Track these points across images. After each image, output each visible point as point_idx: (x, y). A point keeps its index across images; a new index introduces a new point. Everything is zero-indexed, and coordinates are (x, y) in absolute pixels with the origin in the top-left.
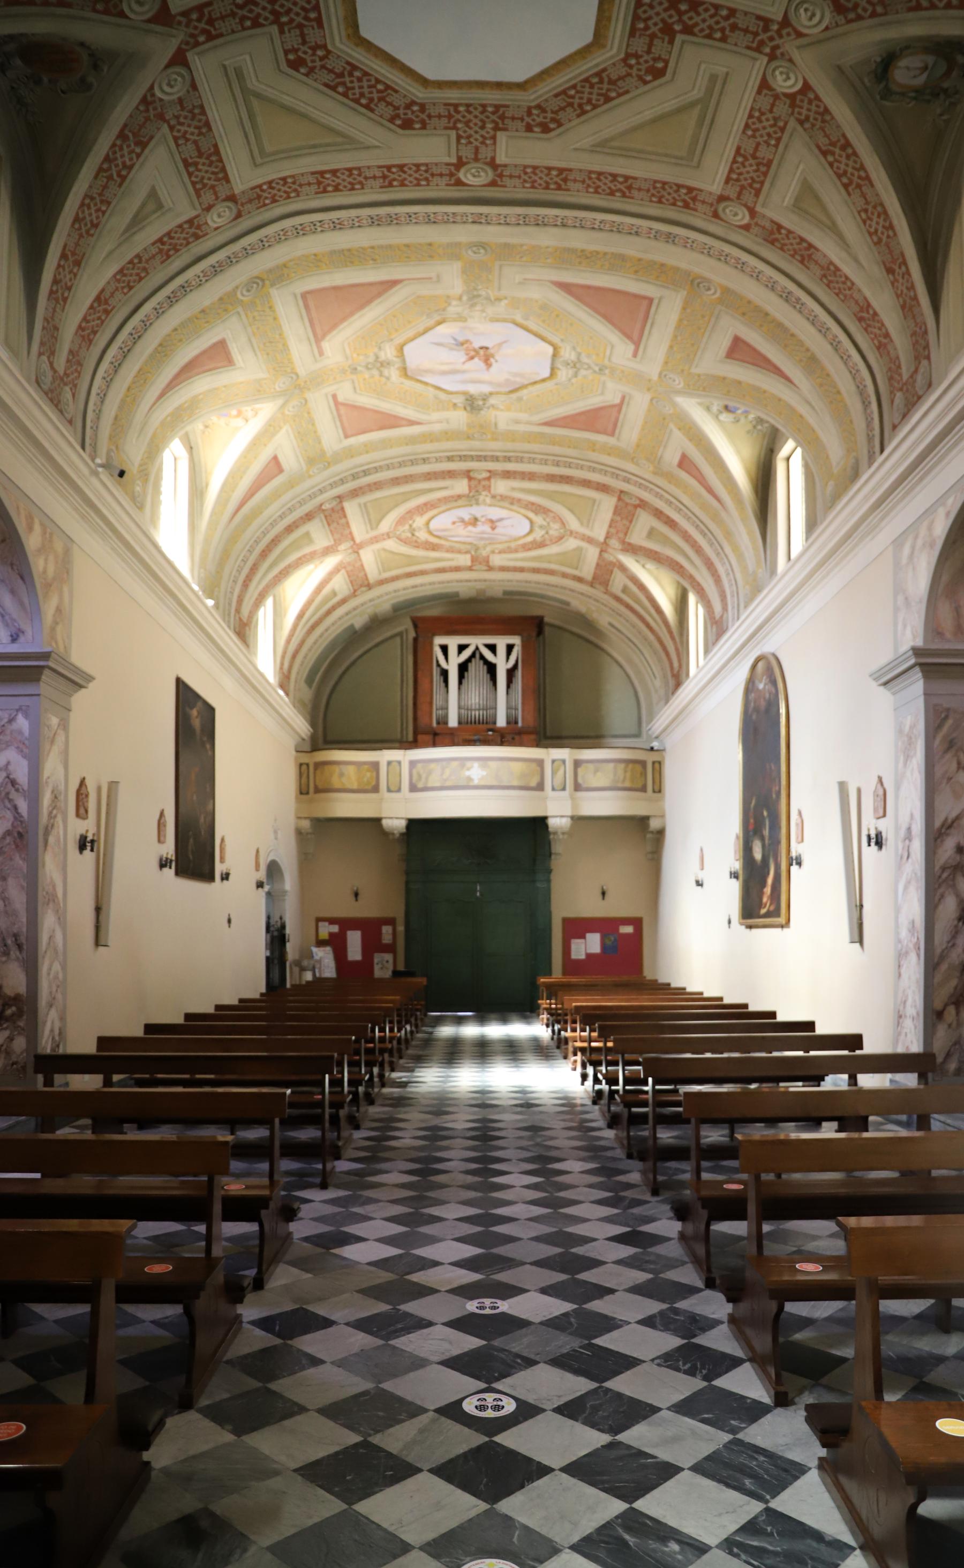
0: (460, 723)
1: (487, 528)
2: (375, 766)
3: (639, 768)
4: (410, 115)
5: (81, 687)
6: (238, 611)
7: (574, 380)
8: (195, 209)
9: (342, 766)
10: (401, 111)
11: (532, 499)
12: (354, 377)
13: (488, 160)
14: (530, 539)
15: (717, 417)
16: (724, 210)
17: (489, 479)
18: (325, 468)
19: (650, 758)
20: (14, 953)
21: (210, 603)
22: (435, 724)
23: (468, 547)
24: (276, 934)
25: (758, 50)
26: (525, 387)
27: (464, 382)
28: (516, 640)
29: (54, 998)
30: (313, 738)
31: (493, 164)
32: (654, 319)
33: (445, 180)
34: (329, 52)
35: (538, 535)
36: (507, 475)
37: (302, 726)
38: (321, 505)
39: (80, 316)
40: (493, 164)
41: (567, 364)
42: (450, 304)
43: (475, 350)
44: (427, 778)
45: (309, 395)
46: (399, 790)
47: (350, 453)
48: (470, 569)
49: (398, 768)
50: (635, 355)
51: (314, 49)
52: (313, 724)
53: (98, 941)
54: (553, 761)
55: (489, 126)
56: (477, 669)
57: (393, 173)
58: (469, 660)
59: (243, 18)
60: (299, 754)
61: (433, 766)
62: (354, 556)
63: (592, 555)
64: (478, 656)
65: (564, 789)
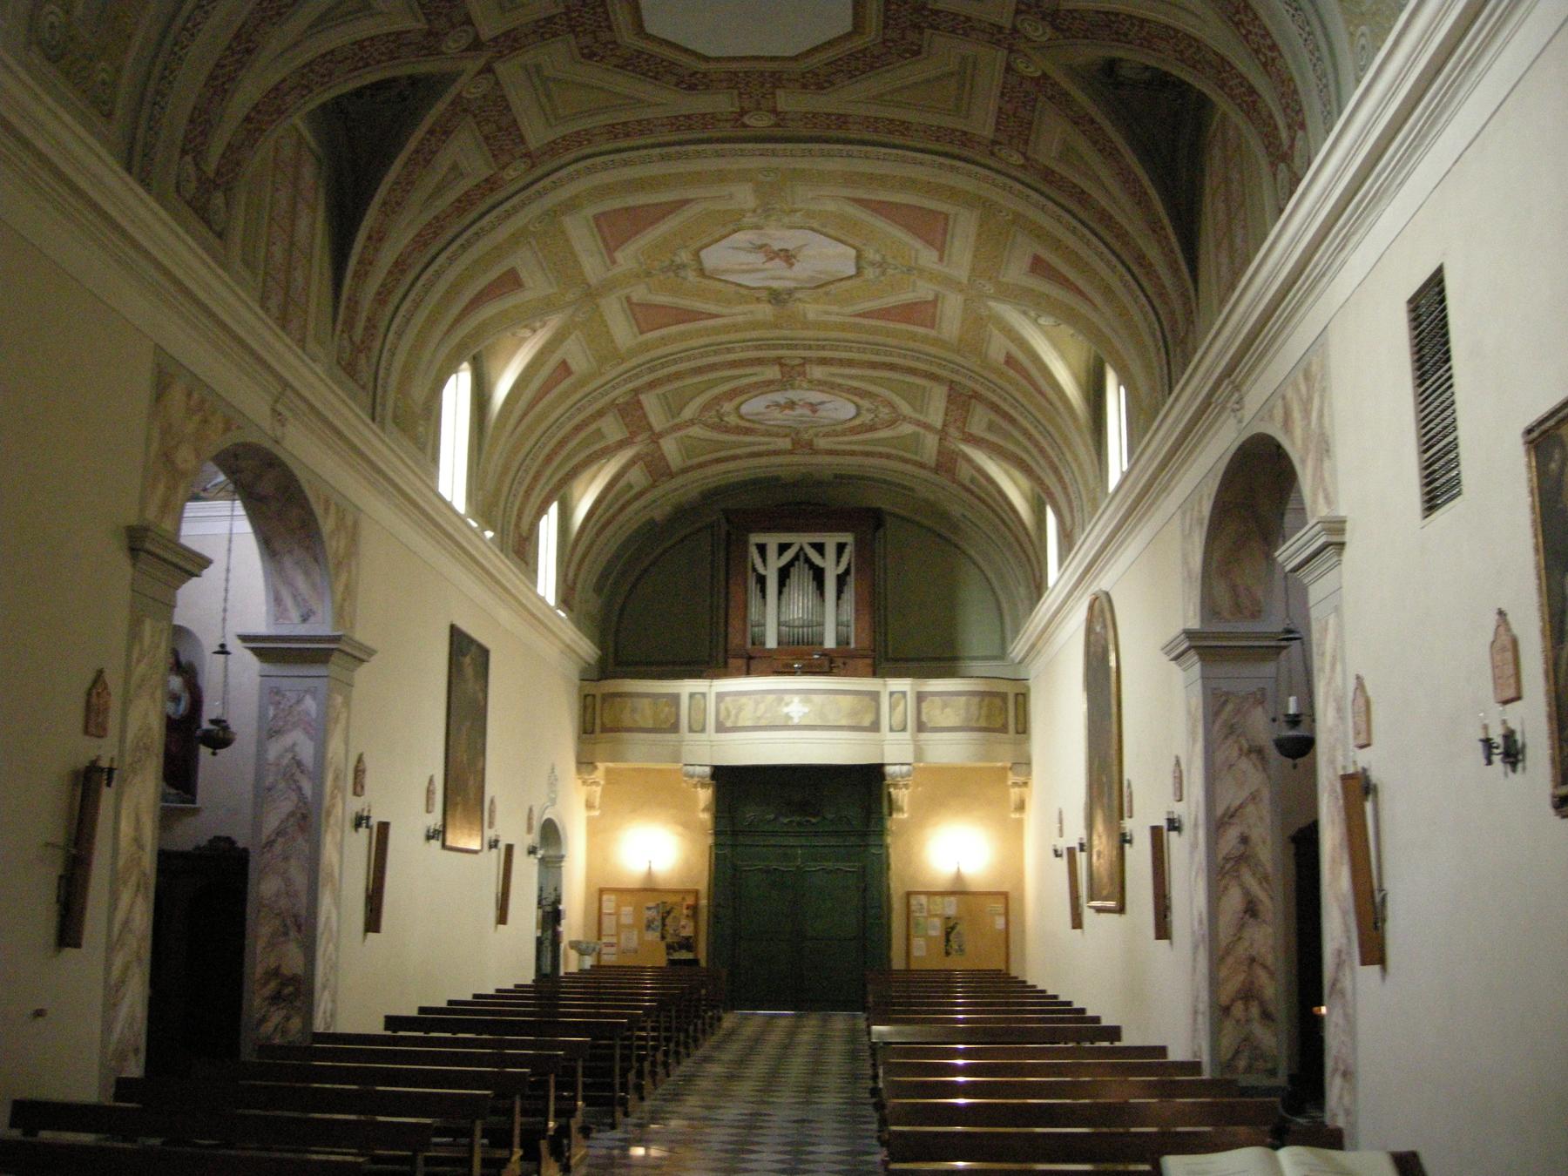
0: (779, 643)
1: (807, 412)
2: (675, 699)
3: (998, 701)
5: (362, 661)
6: (517, 526)
7: (882, 278)
9: (635, 700)
11: (855, 384)
12: (647, 280)
14: (857, 422)
15: (1036, 320)
16: (1000, 150)
17: (803, 365)
18: (619, 364)
19: (1009, 689)
20: (293, 934)
21: (489, 534)
22: (749, 646)
23: (788, 431)
24: (549, 909)
27: (767, 279)
28: (848, 538)
29: (328, 980)
30: (602, 661)
31: (774, 111)
35: (867, 418)
36: (823, 362)
37: (587, 649)
38: (615, 400)
39: (379, 282)
40: (774, 111)
41: (872, 264)
42: (744, 216)
43: (774, 252)
44: (737, 716)
45: (603, 302)
46: (703, 730)
47: (645, 347)
48: (791, 452)
49: (702, 702)
52: (601, 645)
53: (373, 922)
54: (892, 694)
56: (802, 577)
58: (791, 564)
60: (586, 683)
61: (744, 700)
62: (652, 446)
63: (931, 442)
64: (802, 558)
65: (904, 729)
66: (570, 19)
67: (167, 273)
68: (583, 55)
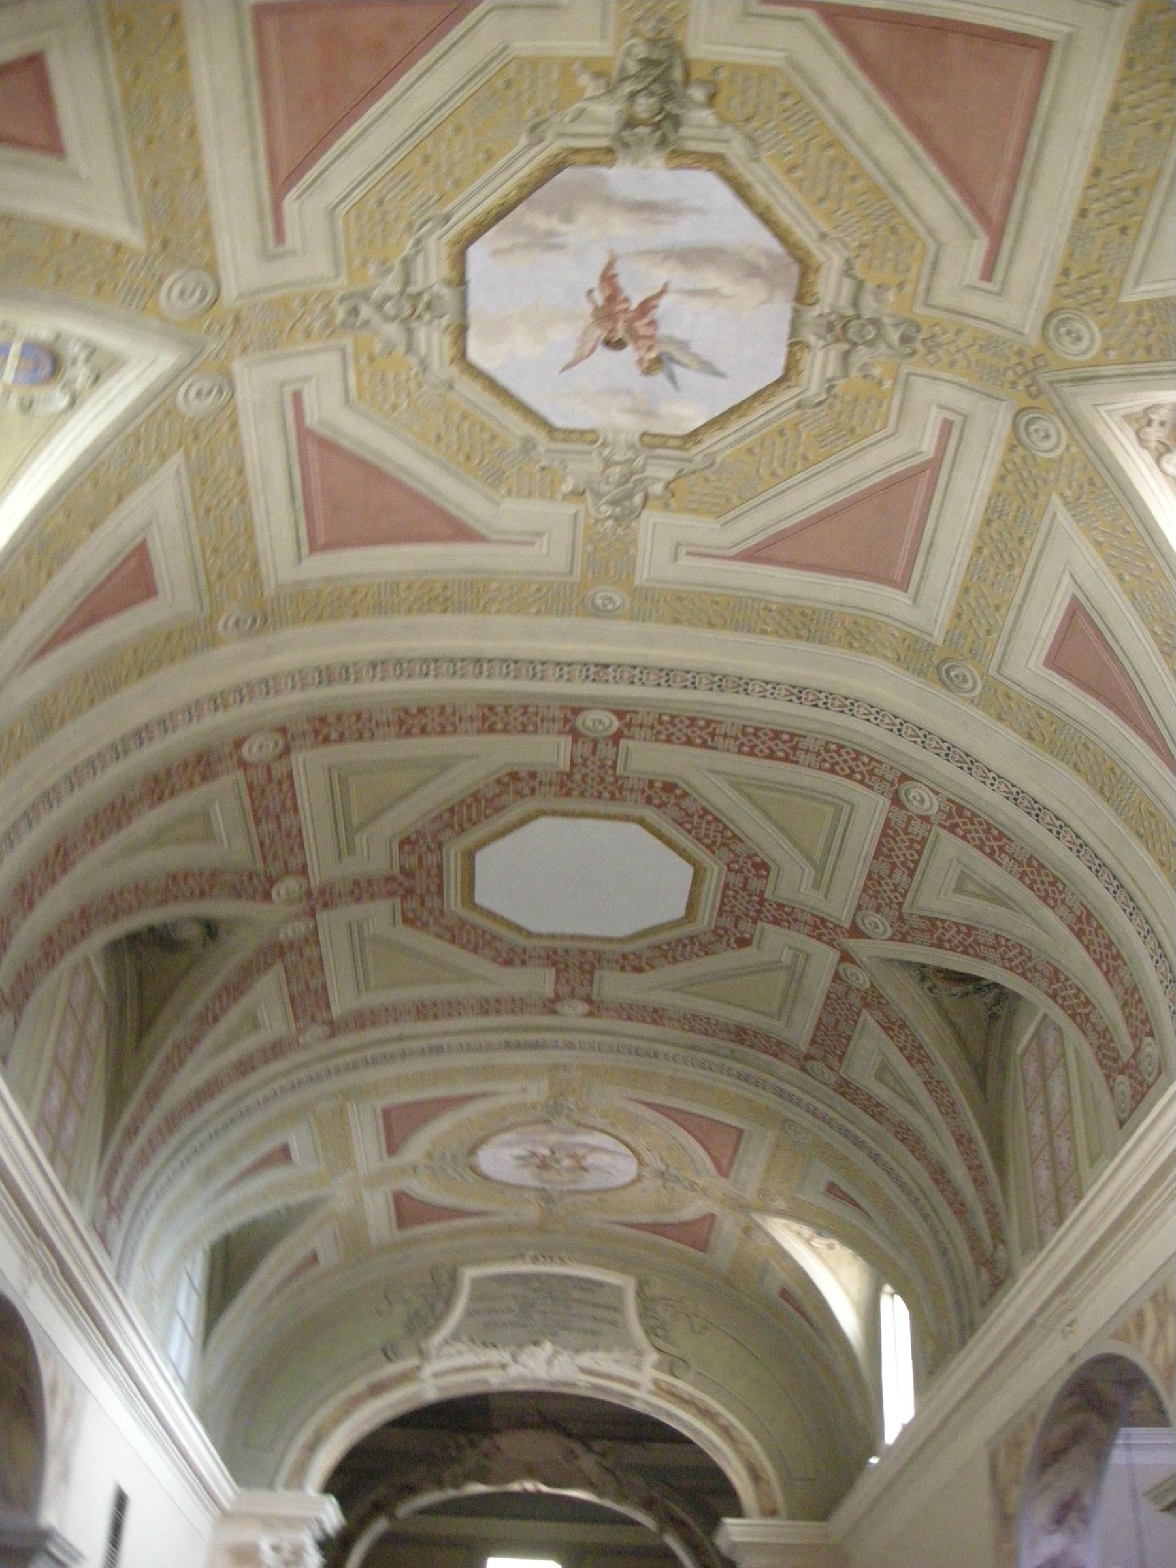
4: (664, 796)
8: (938, 835)
10: (673, 800)
12: (919, 311)
13: (580, 741)
25: (323, 892)
26: (527, 191)
31: (576, 735)
32: (295, 510)
33: (637, 720)
34: (728, 865)
40: (576, 735)
43: (636, 337)
50: (297, 398)
51: (740, 871)
55: (578, 777)
57: (700, 737)
59: (788, 914)
66: (759, 912)
67: (958, 1406)
68: (768, 869)
